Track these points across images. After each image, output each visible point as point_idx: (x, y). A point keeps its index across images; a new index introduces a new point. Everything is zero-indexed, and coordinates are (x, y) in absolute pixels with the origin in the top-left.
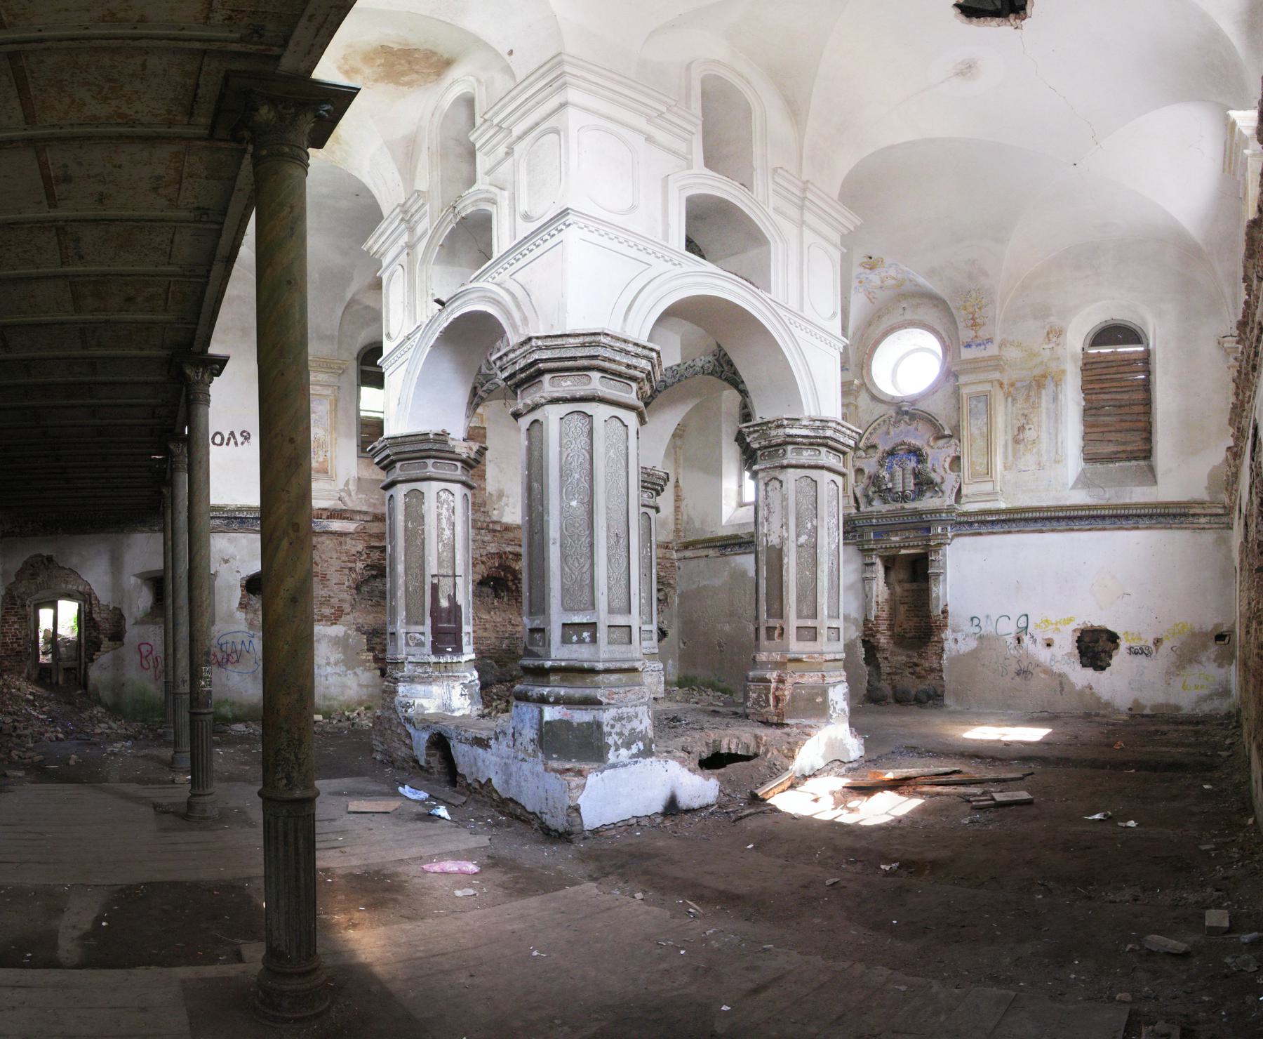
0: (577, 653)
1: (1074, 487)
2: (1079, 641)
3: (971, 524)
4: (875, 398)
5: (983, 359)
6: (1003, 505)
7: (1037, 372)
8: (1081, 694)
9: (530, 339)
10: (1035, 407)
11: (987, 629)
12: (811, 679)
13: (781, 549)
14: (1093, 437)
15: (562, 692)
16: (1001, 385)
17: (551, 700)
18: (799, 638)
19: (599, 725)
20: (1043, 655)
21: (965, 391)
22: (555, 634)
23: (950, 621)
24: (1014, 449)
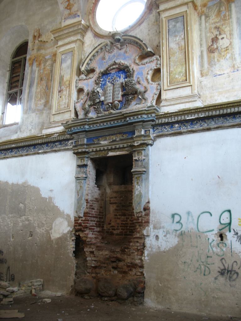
3: (171, 124)
11: (188, 225)
23: (152, 218)
24: (209, 57)
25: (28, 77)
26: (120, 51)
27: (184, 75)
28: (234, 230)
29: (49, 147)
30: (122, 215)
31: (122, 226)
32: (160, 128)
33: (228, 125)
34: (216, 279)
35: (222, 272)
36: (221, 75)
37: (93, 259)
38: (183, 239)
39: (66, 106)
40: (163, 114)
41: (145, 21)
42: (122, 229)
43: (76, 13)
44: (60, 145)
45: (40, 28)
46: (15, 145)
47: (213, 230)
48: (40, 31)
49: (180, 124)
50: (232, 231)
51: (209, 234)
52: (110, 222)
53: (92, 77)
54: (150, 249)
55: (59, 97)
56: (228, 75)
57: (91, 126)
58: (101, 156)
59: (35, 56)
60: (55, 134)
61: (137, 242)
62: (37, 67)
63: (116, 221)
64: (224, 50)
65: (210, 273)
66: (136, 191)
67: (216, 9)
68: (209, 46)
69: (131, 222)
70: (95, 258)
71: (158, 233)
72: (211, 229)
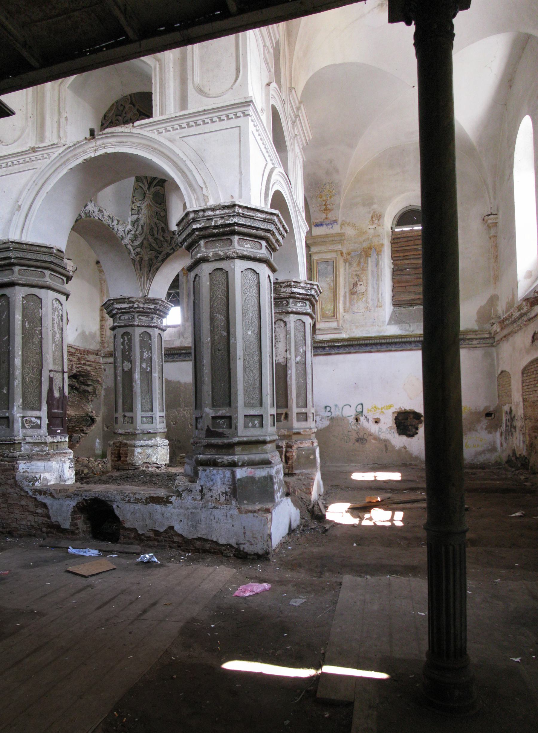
0: (253, 433)
1: (389, 324)
2: (396, 419)
3: (324, 348)
5: (332, 235)
7: (365, 245)
8: (399, 451)
9: (234, 205)
10: (364, 269)
11: (336, 413)
12: (306, 444)
13: (286, 365)
14: (399, 290)
15: (246, 458)
16: (342, 254)
17: (240, 464)
18: (298, 420)
19: (271, 478)
20: (373, 428)
22: (241, 421)
24: (350, 298)
25: (185, 287)
33: (362, 351)
47: (352, 416)
51: (349, 418)
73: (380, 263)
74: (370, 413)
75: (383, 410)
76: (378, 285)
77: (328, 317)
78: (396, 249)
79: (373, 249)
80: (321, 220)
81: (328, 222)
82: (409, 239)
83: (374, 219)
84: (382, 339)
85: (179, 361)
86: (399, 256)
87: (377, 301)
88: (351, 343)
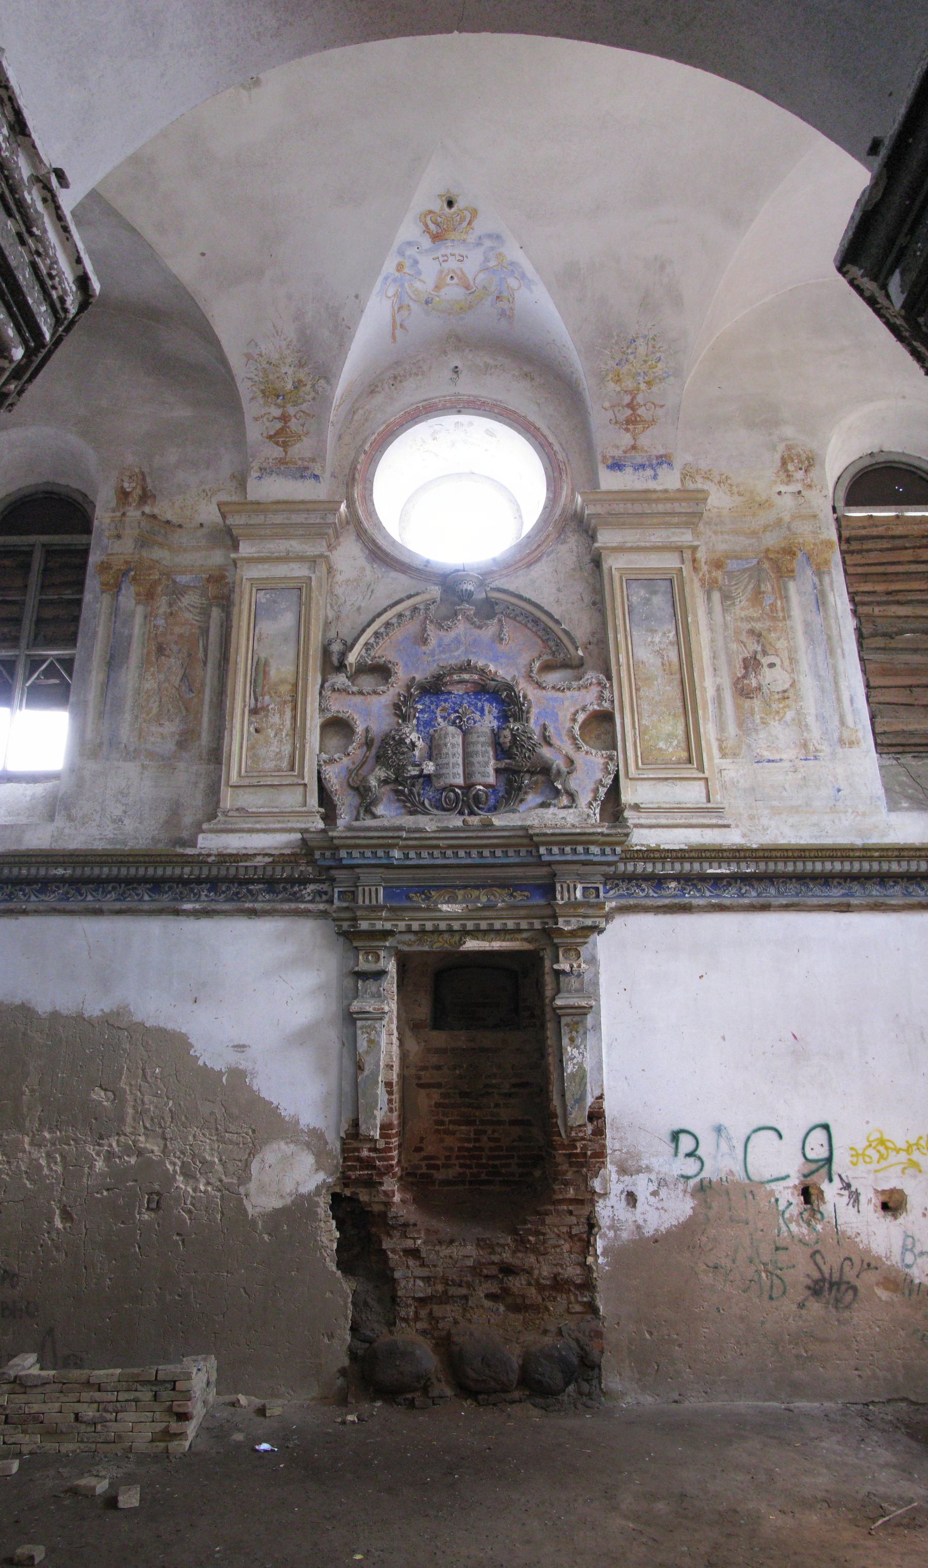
3: (658, 881)
4: (381, 554)
6: (733, 838)
7: (771, 540)
10: (778, 615)
11: (720, 1163)
21: (614, 563)
23: (611, 1141)
24: (738, 707)
25: (101, 630)
26: (477, 631)
27: (683, 745)
28: (840, 1176)
29: (223, 896)
30: (459, 1123)
31: (464, 1157)
32: (624, 886)
33: (815, 901)
34: (801, 1306)
35: (817, 1287)
36: (773, 761)
37: (419, 1272)
38: (706, 1202)
39: (285, 764)
40: (644, 849)
41: (545, 558)
42: (461, 1166)
43: (306, 463)
44: (268, 893)
45: (146, 470)
46: (69, 872)
47: (788, 1176)
48: (148, 480)
49: (682, 882)
50: (836, 1178)
52: (421, 1145)
53: (384, 692)
54: (611, 1234)
55: (252, 730)
56: (791, 764)
57: (412, 854)
58: (436, 947)
59: (126, 562)
60: (259, 858)
61: (571, 1213)
62: (138, 603)
63: (442, 1140)
64: (776, 697)
65: (784, 1293)
66: (567, 1064)
67: (749, 581)
68: (739, 678)
69: (492, 1144)
70: (426, 1269)
71: (634, 1185)
72: (783, 1174)
73: (831, 598)
74: (861, 1167)
75: (916, 1156)
76: (835, 668)
77: (667, 764)
78: (860, 570)
79: (799, 554)
80: (618, 453)
81: (639, 460)
82: (899, 543)
83: (790, 467)
84: (889, 859)
85: (37, 912)
86: (873, 593)
87: (836, 722)
88: (771, 867)
